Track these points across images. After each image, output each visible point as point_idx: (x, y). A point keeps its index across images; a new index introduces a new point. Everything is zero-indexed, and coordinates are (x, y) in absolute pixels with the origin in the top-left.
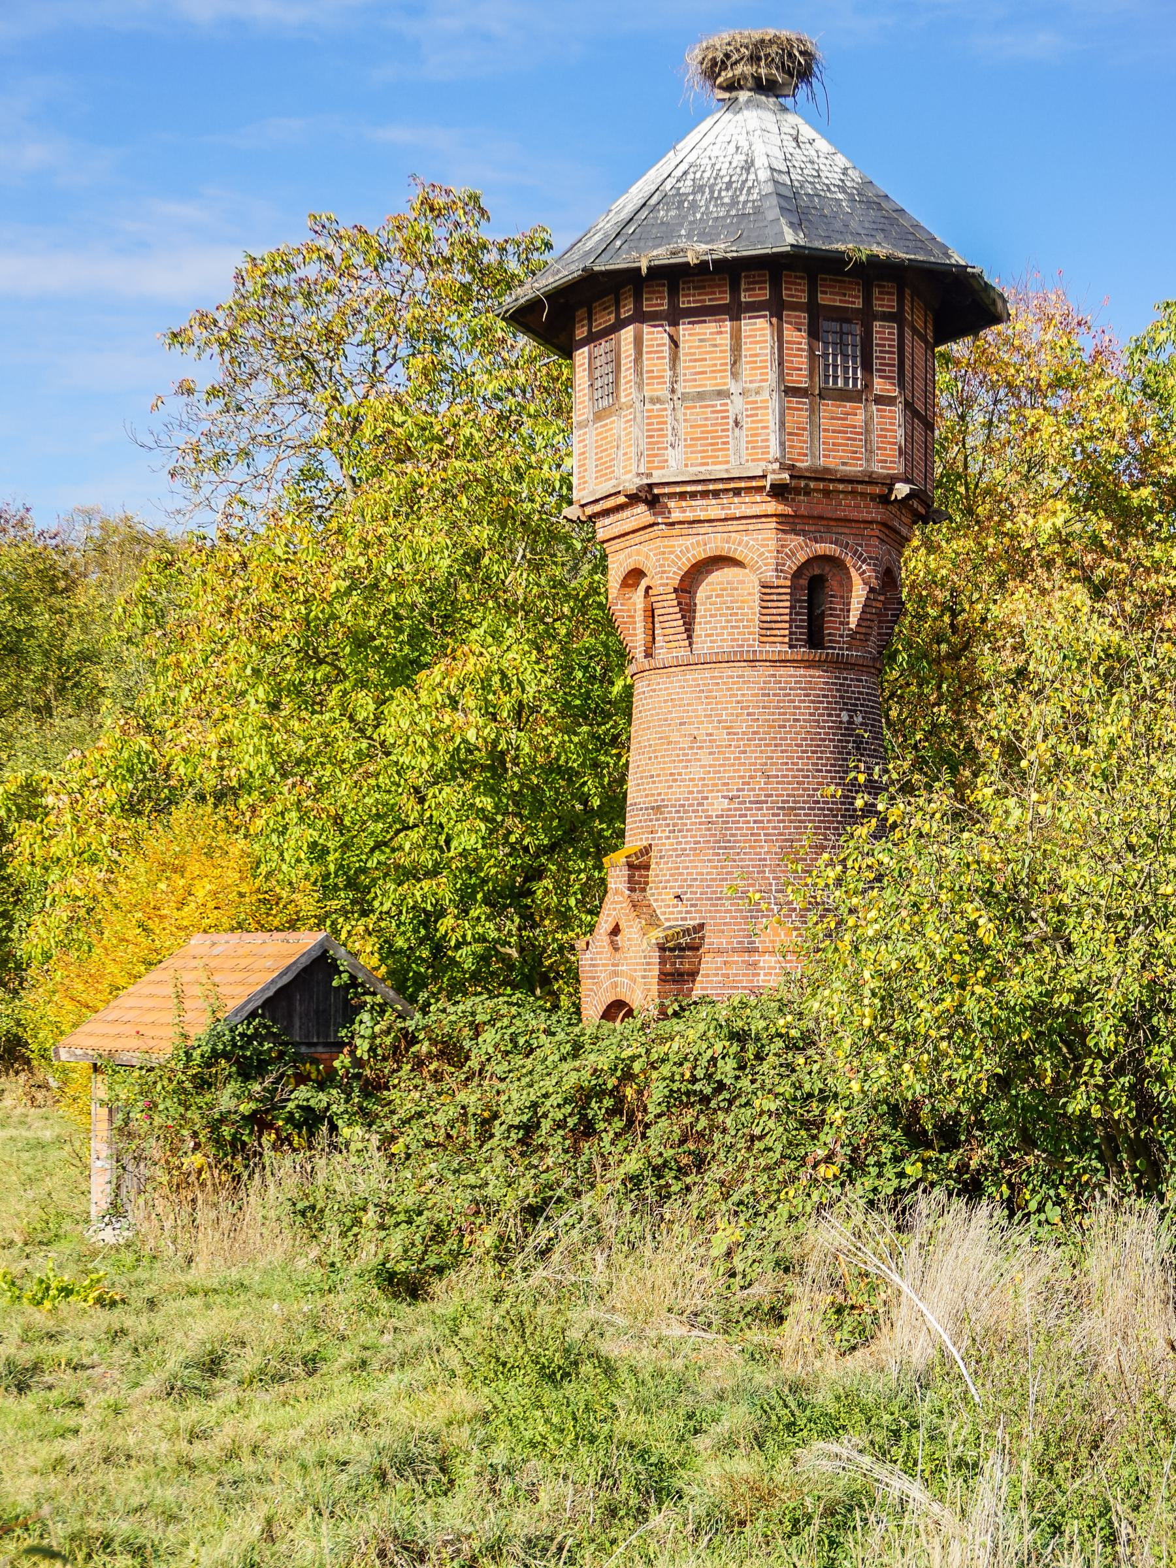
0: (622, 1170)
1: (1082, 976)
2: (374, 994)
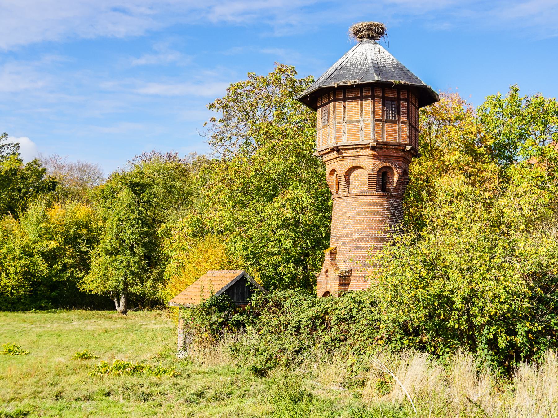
1: (451, 287)
2: (257, 288)
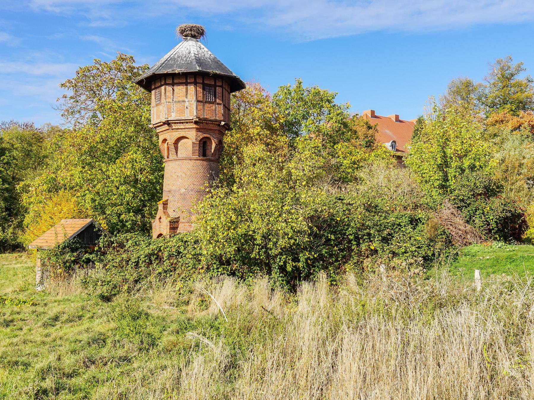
0: (157, 271)
